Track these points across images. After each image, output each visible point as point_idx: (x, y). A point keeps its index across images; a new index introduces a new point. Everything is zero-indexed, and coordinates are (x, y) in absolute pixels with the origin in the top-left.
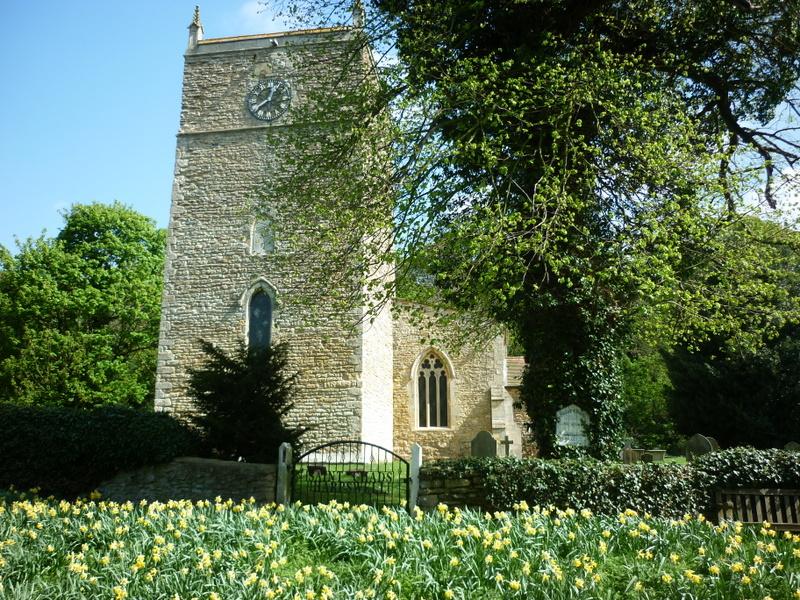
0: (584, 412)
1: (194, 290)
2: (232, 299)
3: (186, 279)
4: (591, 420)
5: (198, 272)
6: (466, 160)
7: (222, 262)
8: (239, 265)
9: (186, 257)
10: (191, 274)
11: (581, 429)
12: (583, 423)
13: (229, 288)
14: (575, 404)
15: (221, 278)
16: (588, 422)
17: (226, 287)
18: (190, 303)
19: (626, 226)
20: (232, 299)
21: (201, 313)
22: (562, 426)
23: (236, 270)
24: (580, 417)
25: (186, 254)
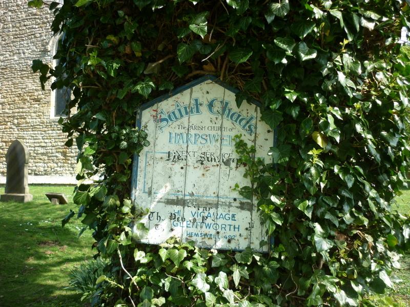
0: (250, 110)
1: (15, 40)
2: (43, 45)
3: (9, 31)
4: (277, 145)
5: (18, 25)
6: (337, 88)
7: (35, 15)
8: (48, 16)
9: (10, 13)
10: (13, 27)
11: (238, 177)
12: (245, 155)
13: (41, 36)
14: (216, 78)
15: (36, 28)
16: (266, 153)
17: (39, 35)
18: (12, 51)
19: (354, 94)
20: (43, 45)
21: (20, 58)
22: (160, 167)
23: (46, 20)
24: (232, 130)
25: (10, 11)
